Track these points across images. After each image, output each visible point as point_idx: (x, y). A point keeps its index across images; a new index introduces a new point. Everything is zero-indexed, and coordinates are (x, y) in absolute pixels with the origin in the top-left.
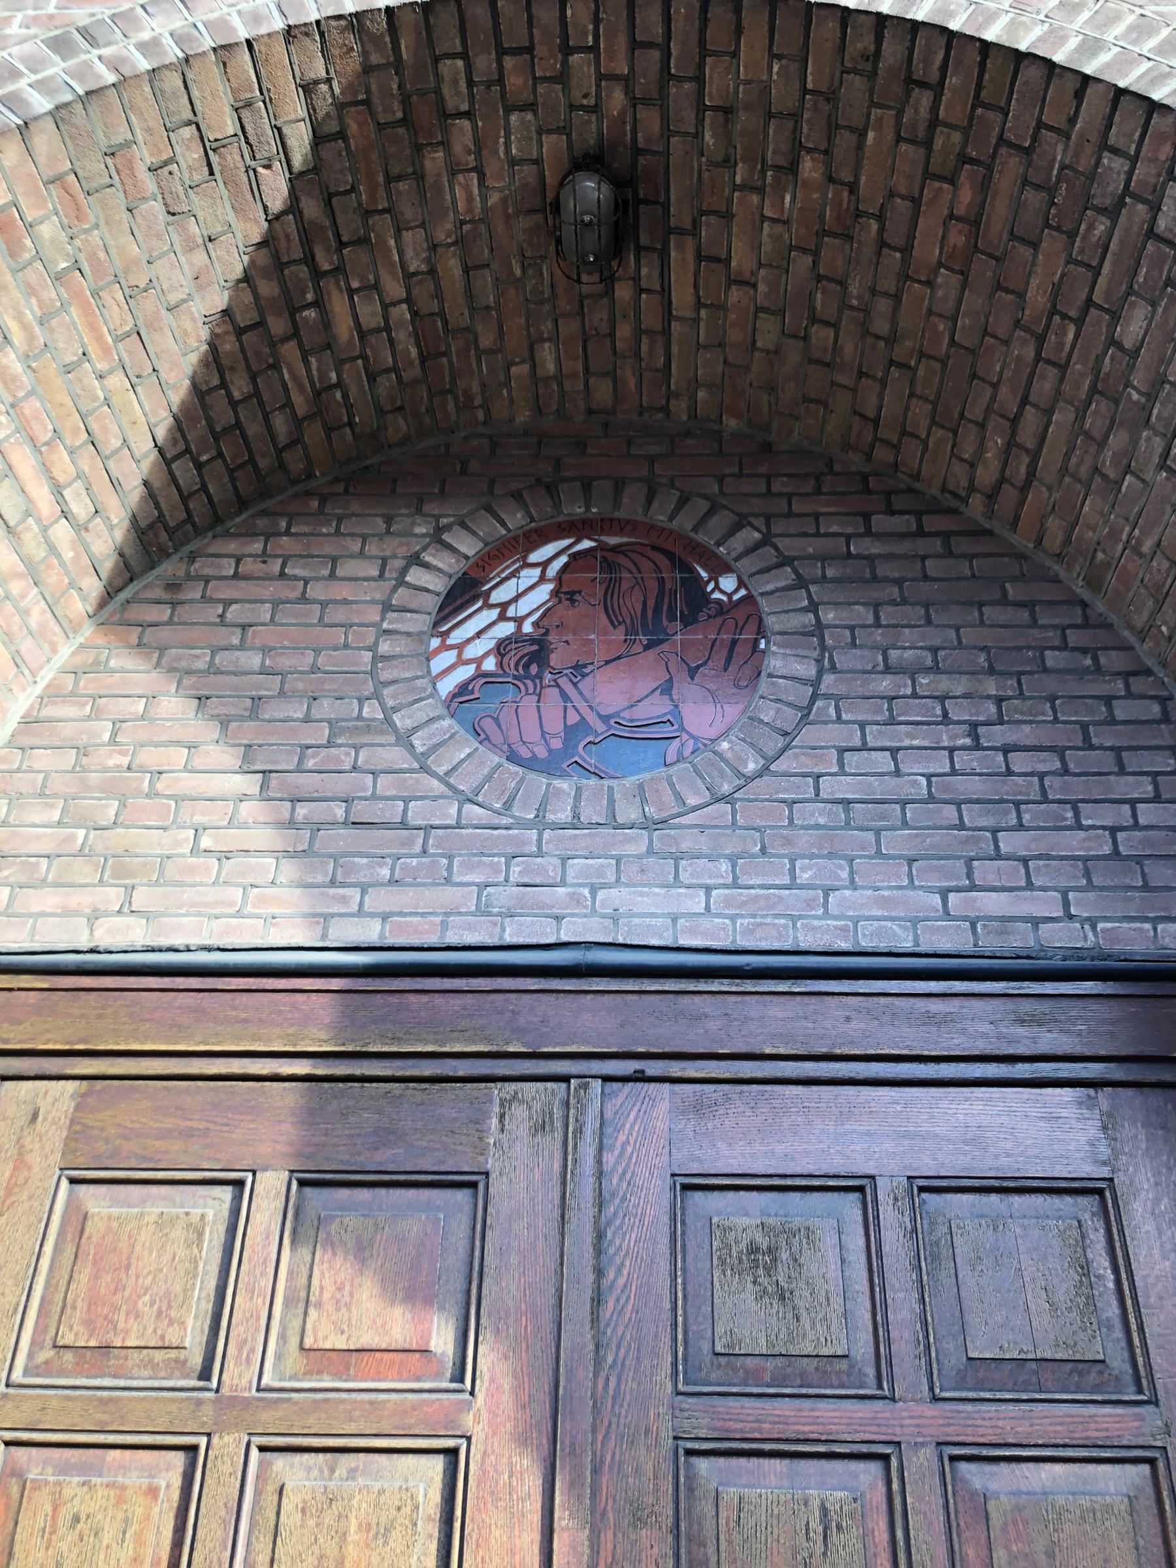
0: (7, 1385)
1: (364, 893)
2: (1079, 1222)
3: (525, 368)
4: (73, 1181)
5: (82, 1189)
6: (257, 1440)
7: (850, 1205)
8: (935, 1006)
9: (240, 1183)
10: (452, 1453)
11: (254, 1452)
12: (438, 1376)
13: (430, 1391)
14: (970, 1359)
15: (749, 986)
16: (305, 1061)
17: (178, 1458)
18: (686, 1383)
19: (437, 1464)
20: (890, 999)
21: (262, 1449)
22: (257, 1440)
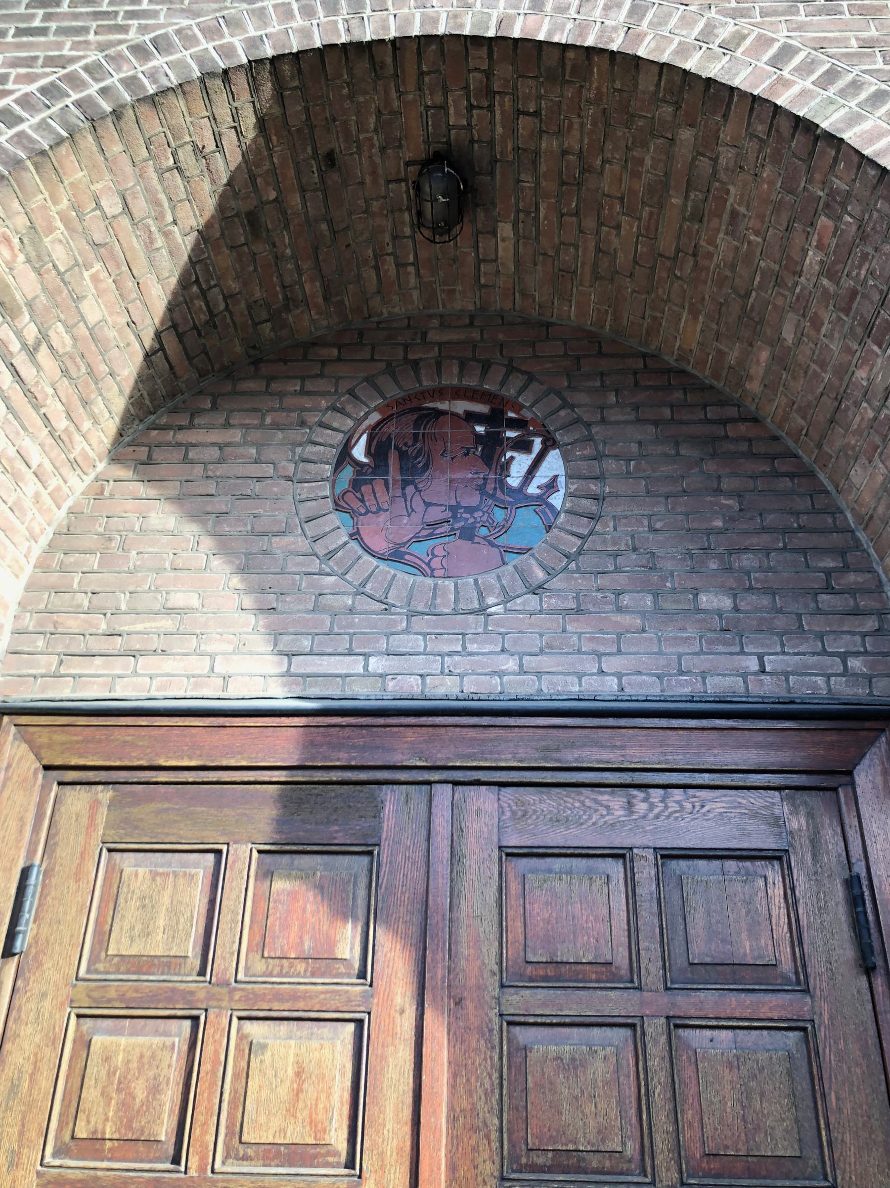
0: (77, 979)
1: (350, 649)
2: (608, 876)
3: (701, 196)
4: (110, 850)
5: (117, 856)
6: (236, 1014)
7: (615, 869)
8: (471, 733)
9: (370, 853)
10: (195, 1019)
11: (235, 1020)
12: (349, 976)
13: (347, 984)
14: (691, 964)
15: (623, 722)
16: (284, 773)
17: (187, 1024)
18: (672, 983)
19: (187, 1024)
20: (587, 731)
21: (240, 1018)
22: (236, 1014)
